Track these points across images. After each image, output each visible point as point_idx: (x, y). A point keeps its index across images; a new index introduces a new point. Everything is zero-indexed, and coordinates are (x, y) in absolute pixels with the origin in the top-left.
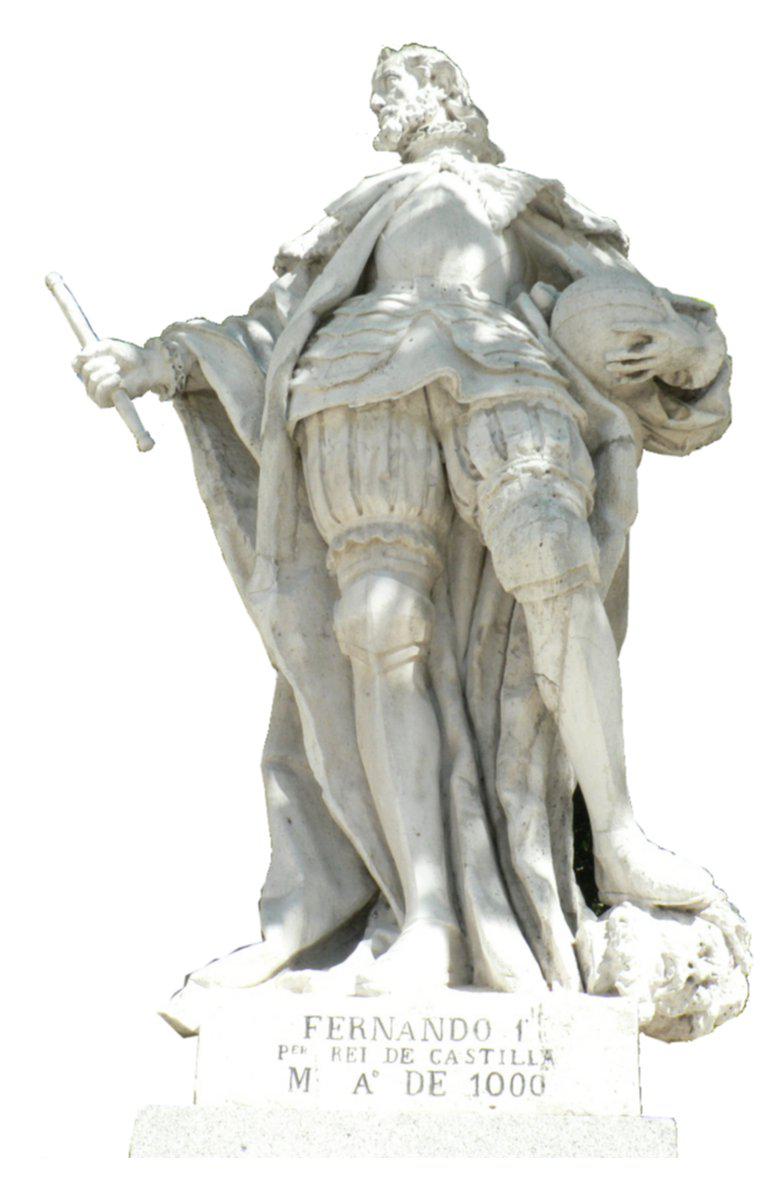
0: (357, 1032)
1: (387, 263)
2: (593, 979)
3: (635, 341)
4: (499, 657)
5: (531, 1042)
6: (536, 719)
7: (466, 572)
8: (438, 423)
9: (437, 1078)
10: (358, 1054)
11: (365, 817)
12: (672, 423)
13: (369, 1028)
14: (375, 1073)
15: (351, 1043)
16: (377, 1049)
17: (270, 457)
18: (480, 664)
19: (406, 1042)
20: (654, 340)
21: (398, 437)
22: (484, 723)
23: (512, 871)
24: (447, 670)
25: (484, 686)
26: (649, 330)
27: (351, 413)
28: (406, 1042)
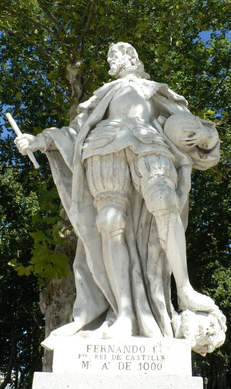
0: (103, 350)
1: (112, 110)
2: (177, 333)
4: (148, 233)
5: (158, 353)
6: (159, 252)
7: (137, 206)
8: (128, 160)
9: (128, 364)
10: (103, 357)
12: (202, 160)
13: (107, 349)
14: (109, 363)
15: (101, 354)
16: (109, 355)
17: (76, 170)
18: (141, 235)
19: (118, 353)
22: (143, 254)
24: (131, 237)
25: (143, 242)
26: (194, 131)
27: (101, 157)
28: (118, 353)
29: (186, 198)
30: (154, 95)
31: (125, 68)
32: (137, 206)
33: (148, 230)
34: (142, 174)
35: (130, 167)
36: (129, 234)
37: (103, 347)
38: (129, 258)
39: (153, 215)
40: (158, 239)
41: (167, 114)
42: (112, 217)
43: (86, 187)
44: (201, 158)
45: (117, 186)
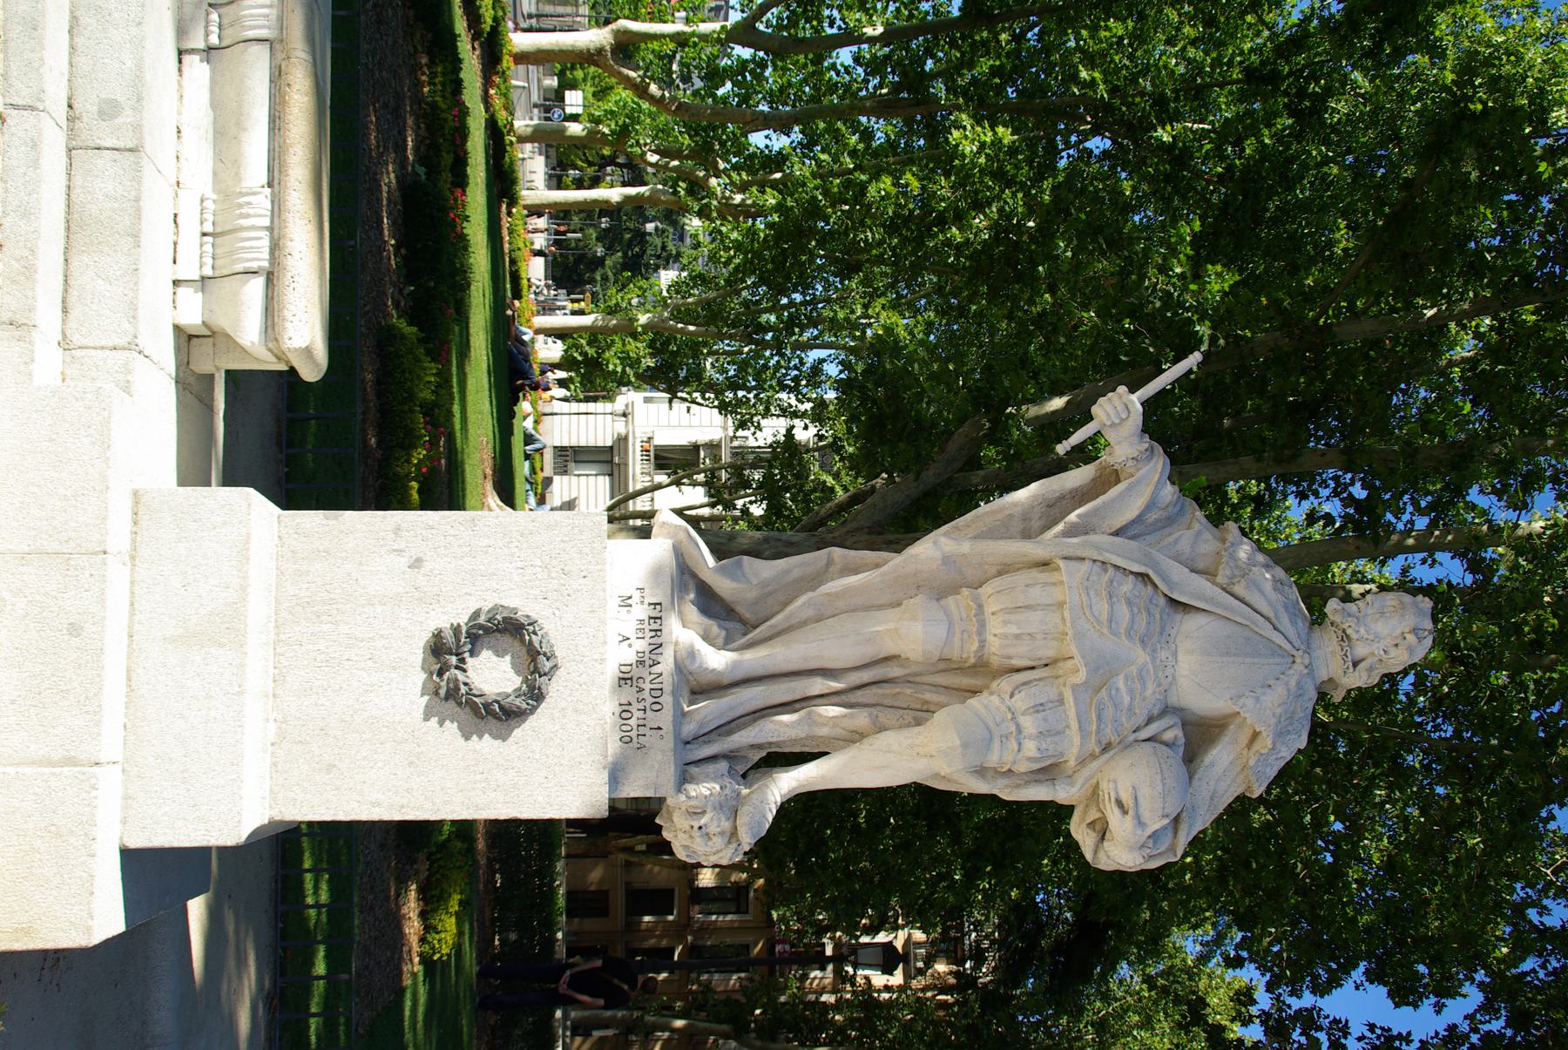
7: (966, 681)
8: (1061, 664)
32: (966, 681)
36: (902, 666)
40: (882, 729)
41: (1191, 758)
42: (913, 633)
43: (1004, 570)
45: (1002, 635)
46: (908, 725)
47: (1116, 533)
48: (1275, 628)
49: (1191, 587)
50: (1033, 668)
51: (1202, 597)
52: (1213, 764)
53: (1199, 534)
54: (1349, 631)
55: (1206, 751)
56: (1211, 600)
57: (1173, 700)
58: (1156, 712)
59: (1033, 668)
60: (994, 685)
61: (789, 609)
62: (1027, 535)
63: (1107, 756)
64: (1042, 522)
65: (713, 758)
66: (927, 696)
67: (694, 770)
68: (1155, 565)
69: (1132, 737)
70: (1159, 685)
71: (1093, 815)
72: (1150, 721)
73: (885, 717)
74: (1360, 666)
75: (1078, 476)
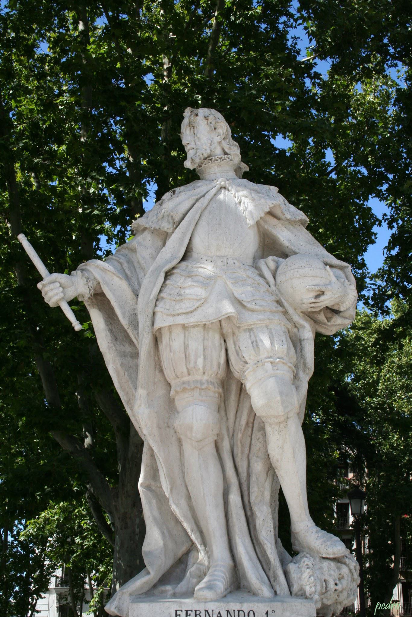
1: (198, 244)
2: (293, 593)
3: (316, 294)
4: (249, 439)
6: (267, 470)
7: (233, 397)
8: (225, 331)
11: (189, 512)
12: (329, 324)
17: (144, 344)
18: (241, 443)
20: (325, 293)
21: (207, 340)
22: (243, 470)
23: (257, 539)
24: (226, 445)
25: (242, 452)
26: (323, 289)
27: (185, 327)
29: (305, 388)
30: (261, 218)
31: (210, 160)
32: (233, 397)
33: (249, 433)
34: (247, 359)
35: (227, 341)
36: (222, 440)
37: (198, 612)
38: (222, 478)
39: (255, 414)
41: (284, 254)
42: (197, 416)
44: (328, 321)
46: (265, 435)
47: (137, 295)
48: (203, 196)
49: (175, 246)
50: (226, 350)
51: (182, 239)
52: (289, 241)
53: (139, 243)
54: (206, 156)
55: (281, 245)
56: (184, 234)
57: (249, 261)
58: (257, 272)
59: (226, 350)
60: (236, 375)
61: (181, 518)
62: (135, 355)
63: (285, 304)
64: (127, 345)
65: (286, 574)
66: (243, 422)
67: (295, 588)
68: (159, 268)
69: (273, 287)
70: (240, 267)
71: (322, 317)
72: (262, 276)
73: (257, 446)
74: (228, 151)
75: (97, 319)
